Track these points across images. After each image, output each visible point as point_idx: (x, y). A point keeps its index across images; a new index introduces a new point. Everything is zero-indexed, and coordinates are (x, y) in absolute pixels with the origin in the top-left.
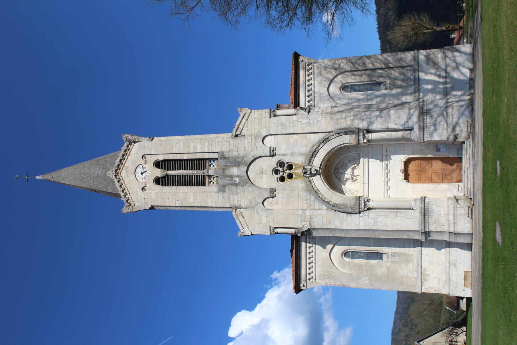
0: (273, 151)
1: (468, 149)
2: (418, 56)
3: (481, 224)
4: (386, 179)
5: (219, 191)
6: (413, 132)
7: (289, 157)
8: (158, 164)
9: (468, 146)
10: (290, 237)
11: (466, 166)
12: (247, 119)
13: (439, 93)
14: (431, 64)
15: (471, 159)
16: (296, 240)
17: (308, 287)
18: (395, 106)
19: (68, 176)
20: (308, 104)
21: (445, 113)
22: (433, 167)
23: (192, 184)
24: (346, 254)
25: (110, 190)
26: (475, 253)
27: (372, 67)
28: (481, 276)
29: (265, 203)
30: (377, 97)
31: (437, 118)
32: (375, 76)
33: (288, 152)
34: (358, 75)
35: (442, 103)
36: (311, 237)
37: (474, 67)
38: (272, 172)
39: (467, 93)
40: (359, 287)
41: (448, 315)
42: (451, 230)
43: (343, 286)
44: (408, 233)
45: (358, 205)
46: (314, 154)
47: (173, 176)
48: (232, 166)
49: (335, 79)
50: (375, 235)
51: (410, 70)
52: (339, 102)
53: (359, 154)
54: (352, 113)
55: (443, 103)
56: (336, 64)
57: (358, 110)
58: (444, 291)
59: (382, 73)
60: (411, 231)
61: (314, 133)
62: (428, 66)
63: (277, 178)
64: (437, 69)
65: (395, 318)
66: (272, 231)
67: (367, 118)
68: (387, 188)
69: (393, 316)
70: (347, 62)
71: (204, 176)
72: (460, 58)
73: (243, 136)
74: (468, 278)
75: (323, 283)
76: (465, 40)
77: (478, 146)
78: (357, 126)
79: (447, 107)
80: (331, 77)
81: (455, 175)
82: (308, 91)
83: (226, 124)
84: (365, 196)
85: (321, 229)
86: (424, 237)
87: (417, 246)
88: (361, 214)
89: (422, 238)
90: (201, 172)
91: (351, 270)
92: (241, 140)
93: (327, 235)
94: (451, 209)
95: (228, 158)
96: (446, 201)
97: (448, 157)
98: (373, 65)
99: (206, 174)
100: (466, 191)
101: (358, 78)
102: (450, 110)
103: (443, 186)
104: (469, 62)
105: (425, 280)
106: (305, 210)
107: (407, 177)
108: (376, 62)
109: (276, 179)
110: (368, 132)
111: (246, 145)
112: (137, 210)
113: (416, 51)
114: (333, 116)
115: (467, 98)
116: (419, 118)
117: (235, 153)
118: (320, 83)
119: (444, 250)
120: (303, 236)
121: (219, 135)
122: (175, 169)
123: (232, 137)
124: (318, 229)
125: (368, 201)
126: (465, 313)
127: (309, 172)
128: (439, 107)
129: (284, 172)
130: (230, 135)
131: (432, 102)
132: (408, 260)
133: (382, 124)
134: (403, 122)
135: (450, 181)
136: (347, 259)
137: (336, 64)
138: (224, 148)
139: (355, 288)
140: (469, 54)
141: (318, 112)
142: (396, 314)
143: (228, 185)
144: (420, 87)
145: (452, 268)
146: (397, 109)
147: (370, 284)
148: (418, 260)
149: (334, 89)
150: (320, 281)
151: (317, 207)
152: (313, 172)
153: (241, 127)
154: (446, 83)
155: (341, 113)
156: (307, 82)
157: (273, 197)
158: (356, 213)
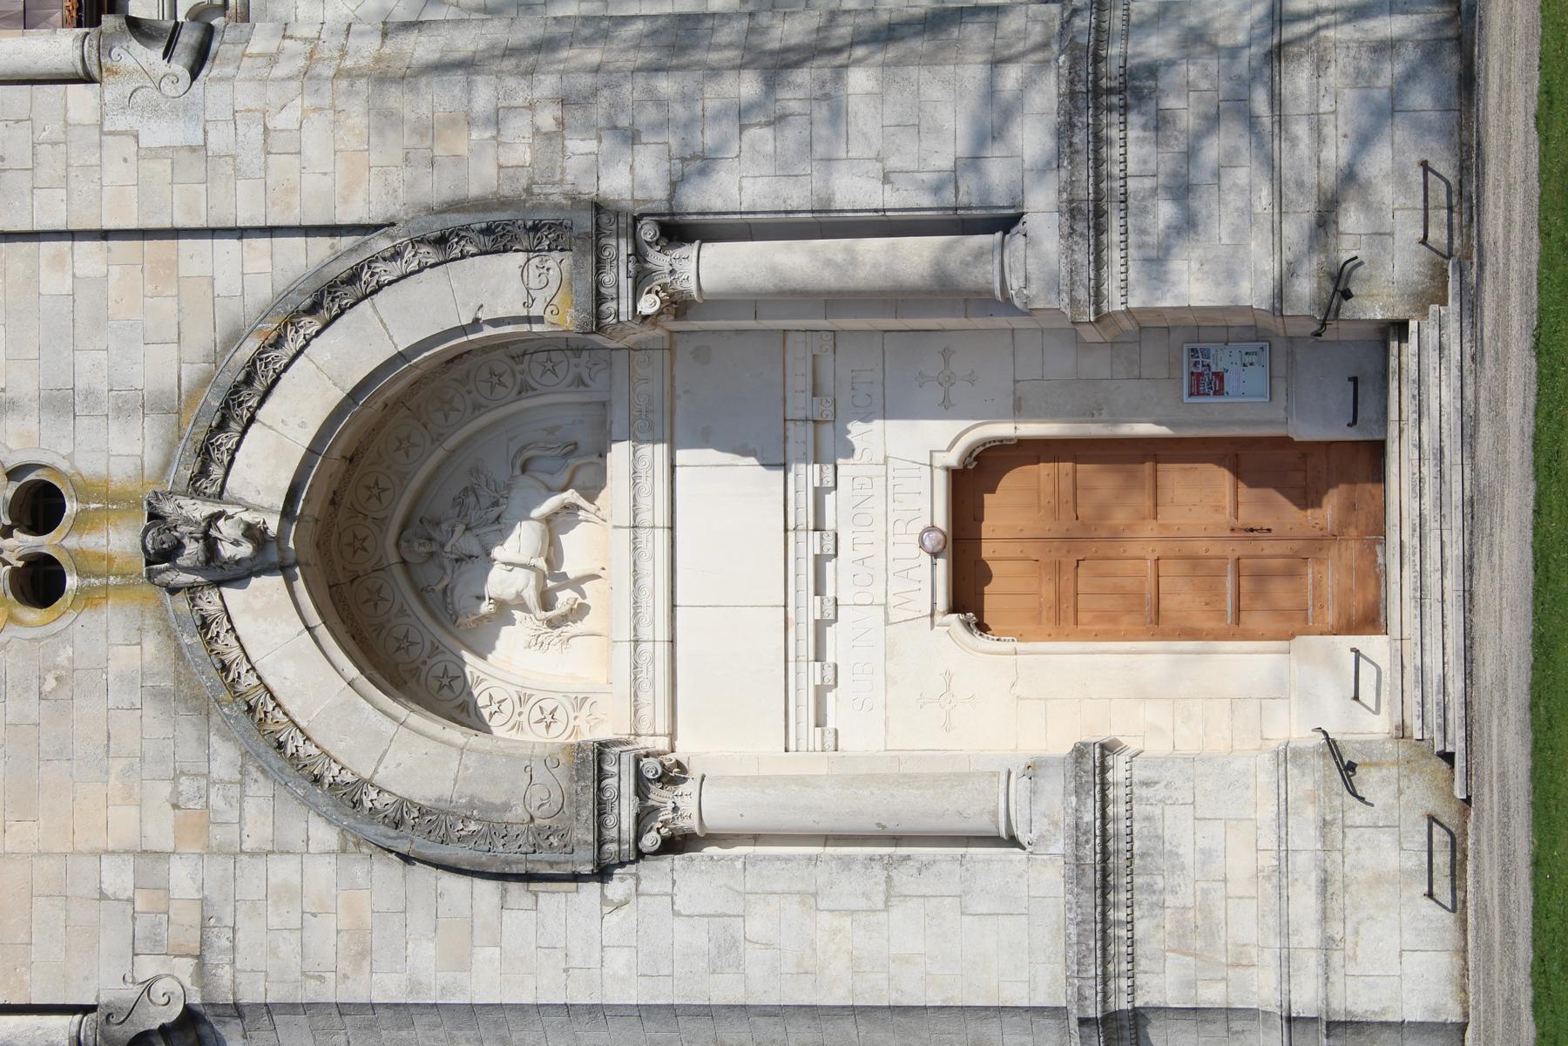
4: (812, 608)
6: (1016, 242)
9: (1432, 357)
22: (1168, 515)
45: (587, 812)
46: (237, 401)
53: (604, 404)
54: (547, 84)
57: (593, 56)
60: (1001, 1010)
61: (241, 232)
67: (657, 127)
68: (813, 674)
78: (587, 189)
81: (1330, 578)
85: (292, 1008)
88: (617, 887)
96: (1266, 779)
97: (1285, 442)
100: (1413, 696)
103: (1246, 663)
107: (967, 595)
110: (678, 231)
114: (395, 98)
124: (269, 1008)
125: (672, 776)
127: (193, 549)
133: (785, 170)
141: (272, 59)
151: (258, 831)
152: (227, 551)
155: (459, 76)
158: (576, 878)
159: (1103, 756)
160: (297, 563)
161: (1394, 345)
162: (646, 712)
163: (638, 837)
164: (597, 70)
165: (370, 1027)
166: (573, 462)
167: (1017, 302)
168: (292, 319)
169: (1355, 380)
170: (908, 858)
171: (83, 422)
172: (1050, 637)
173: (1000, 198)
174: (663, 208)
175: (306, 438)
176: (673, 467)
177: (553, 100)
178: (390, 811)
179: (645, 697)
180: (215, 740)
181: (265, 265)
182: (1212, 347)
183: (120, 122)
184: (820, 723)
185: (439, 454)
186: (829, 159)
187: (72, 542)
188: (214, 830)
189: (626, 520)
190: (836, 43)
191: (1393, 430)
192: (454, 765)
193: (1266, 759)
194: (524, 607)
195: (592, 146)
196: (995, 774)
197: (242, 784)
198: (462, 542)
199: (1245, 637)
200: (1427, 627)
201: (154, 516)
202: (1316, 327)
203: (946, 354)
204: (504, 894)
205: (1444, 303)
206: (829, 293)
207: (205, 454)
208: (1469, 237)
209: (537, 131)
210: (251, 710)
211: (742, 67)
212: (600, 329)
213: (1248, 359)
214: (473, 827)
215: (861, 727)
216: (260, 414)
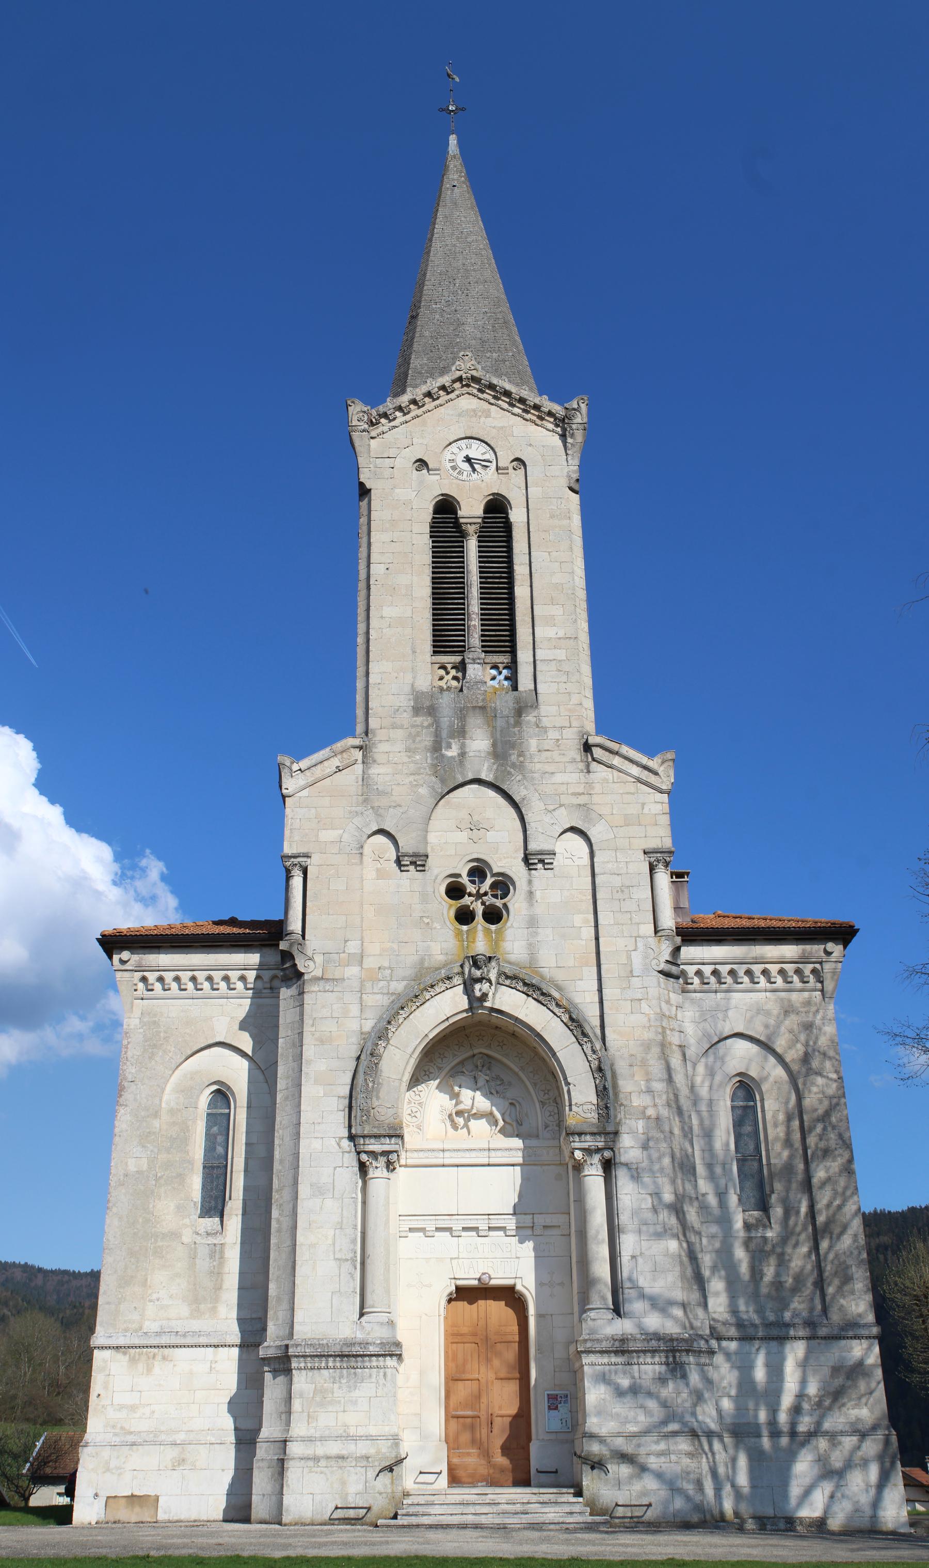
0: (541, 861)
1: (557, 1509)
2: (856, 1337)
3: (312, 1553)
4: (457, 1226)
5: (417, 696)
6: (610, 1315)
7: (524, 912)
8: (497, 507)
9: (567, 1509)
10: (277, 916)
11: (502, 1499)
12: (639, 780)
13: (740, 1409)
14: (839, 1381)
15: (526, 1519)
16: (268, 937)
17: (119, 974)
18: (692, 1256)
19: (459, 232)
20: (691, 970)
21: (673, 1427)
22: (498, 1384)
23: (438, 613)
24: (222, 1095)
25: (416, 362)
26: (212, 1534)
27: (815, 1181)
28: (141, 1553)
29: (380, 838)
30: (722, 1196)
31: (658, 1398)
32: (788, 1190)
33: (539, 910)
34: (788, 1133)
35: (707, 1416)
36: (276, 983)
37: (833, 1533)
38: (477, 860)
39: (744, 1509)
40: (117, 1139)
41: (14, 1445)
42: (294, 1449)
43: (121, 1090)
44: (286, 1298)
45: (376, 1131)
46: (536, 990)
47: (461, 554)
48: (493, 735)
49: (772, 1060)
50: (280, 1190)
51: (812, 1309)
52: (701, 1069)
53: (537, 1136)
54: (665, 1112)
55: (708, 1420)
56: (822, 1062)
57: (677, 1131)
58: (95, 1426)
59: (798, 1212)
60: (293, 1309)
61: (600, 990)
62: (826, 1371)
63: (459, 876)
64: (819, 1404)
65: (14, 1265)
66: (296, 861)
67: (650, 1157)
68: (431, 1227)
69: (20, 1258)
70: (831, 1098)
71: (461, 650)
72: (861, 1483)
73: (588, 766)
74: (137, 1509)
75: (132, 1022)
76: (919, 1507)
77: (567, 1542)
78: (623, 1129)
79: (694, 1434)
80: (780, 1045)
81: (472, 1460)
82: (732, 973)
83: (625, 714)
84: (403, 1155)
85: (302, 1014)
86: (271, 1353)
87: (242, 1331)
88: (346, 1144)
89: (269, 1347)
90: (475, 639)
91: (172, 1112)
92: (573, 761)
93: (282, 1032)
94: (363, 1448)
95: (518, 723)
96: (386, 1430)
97: (529, 1439)
98: (823, 1184)
99: (469, 656)
100: (421, 1500)
101: (781, 1131)
102: (683, 1445)
103: (435, 1421)
104: (850, 1518)
105: (133, 1361)
106: (361, 963)
108: (835, 1193)
110: (608, 1166)
111: (559, 778)
112: (358, 449)
113: (875, 1330)
114: (656, 1050)
115: (728, 1506)
116: (657, 1336)
117: (533, 744)
118: (759, 1010)
119: (228, 1423)
120: (279, 958)
121: (589, 693)
122: (483, 558)
123: (584, 734)
124: (302, 1005)
125: (390, 1166)
126: (23, 1504)
127: (478, 973)
128: (695, 1405)
129: (479, 896)
130: (591, 727)
131: (709, 1382)
132: (201, 1299)
133: (635, 1213)
135: (452, 1442)
136: (204, 1098)
137: (822, 1062)
138: (550, 710)
139: (114, 1127)
140: (874, 1517)
141: (668, 1002)
142: (26, 1268)
143: (437, 723)
144: (757, 1343)
145: (171, 1453)
146: (681, 1263)
147: (126, 1175)
148: (199, 1334)
149: (741, 1055)
150: (137, 1013)
151: (370, 1000)
152: (477, 986)
153: (616, 761)
154: (775, 1434)
155: (666, 1076)
156: (762, 967)
157: (398, 862)
158: (350, 1127)
159: (396, 1355)
160: (473, 1014)
161: (572, 1491)
162: (415, 1155)
163: (365, 1152)
164: (671, 1132)
165: (294, 1045)
166: (514, 1124)
167: (584, 1315)
168: (567, 1011)
169: (556, 1472)
171: (526, 931)
172: (446, 1331)
174: (617, 1161)
176: (513, 1165)
177: (658, 1114)
178: (377, 1051)
179: (421, 1154)
180: (405, 983)
181: (588, 1000)
182: (568, 1405)
183: (640, 944)
184: (411, 1230)
185: (516, 1070)
186: (640, 1232)
189: (492, 1146)
190: (688, 1234)
191: (535, 1490)
192: (394, 1077)
193: (395, 1430)
194: (457, 1104)
195: (641, 1130)
197: (388, 993)
199: (447, 1421)
200: (451, 1506)
201: (490, 959)
202: (578, 1453)
203: (562, 1284)
204: (344, 1097)
205: (591, 1515)
207: (514, 978)
208: (619, 1527)
209: (645, 1108)
210: (416, 997)
211: (676, 1194)
212: (568, 1134)
213: (564, 1421)
214: (371, 1085)
216: (530, 999)
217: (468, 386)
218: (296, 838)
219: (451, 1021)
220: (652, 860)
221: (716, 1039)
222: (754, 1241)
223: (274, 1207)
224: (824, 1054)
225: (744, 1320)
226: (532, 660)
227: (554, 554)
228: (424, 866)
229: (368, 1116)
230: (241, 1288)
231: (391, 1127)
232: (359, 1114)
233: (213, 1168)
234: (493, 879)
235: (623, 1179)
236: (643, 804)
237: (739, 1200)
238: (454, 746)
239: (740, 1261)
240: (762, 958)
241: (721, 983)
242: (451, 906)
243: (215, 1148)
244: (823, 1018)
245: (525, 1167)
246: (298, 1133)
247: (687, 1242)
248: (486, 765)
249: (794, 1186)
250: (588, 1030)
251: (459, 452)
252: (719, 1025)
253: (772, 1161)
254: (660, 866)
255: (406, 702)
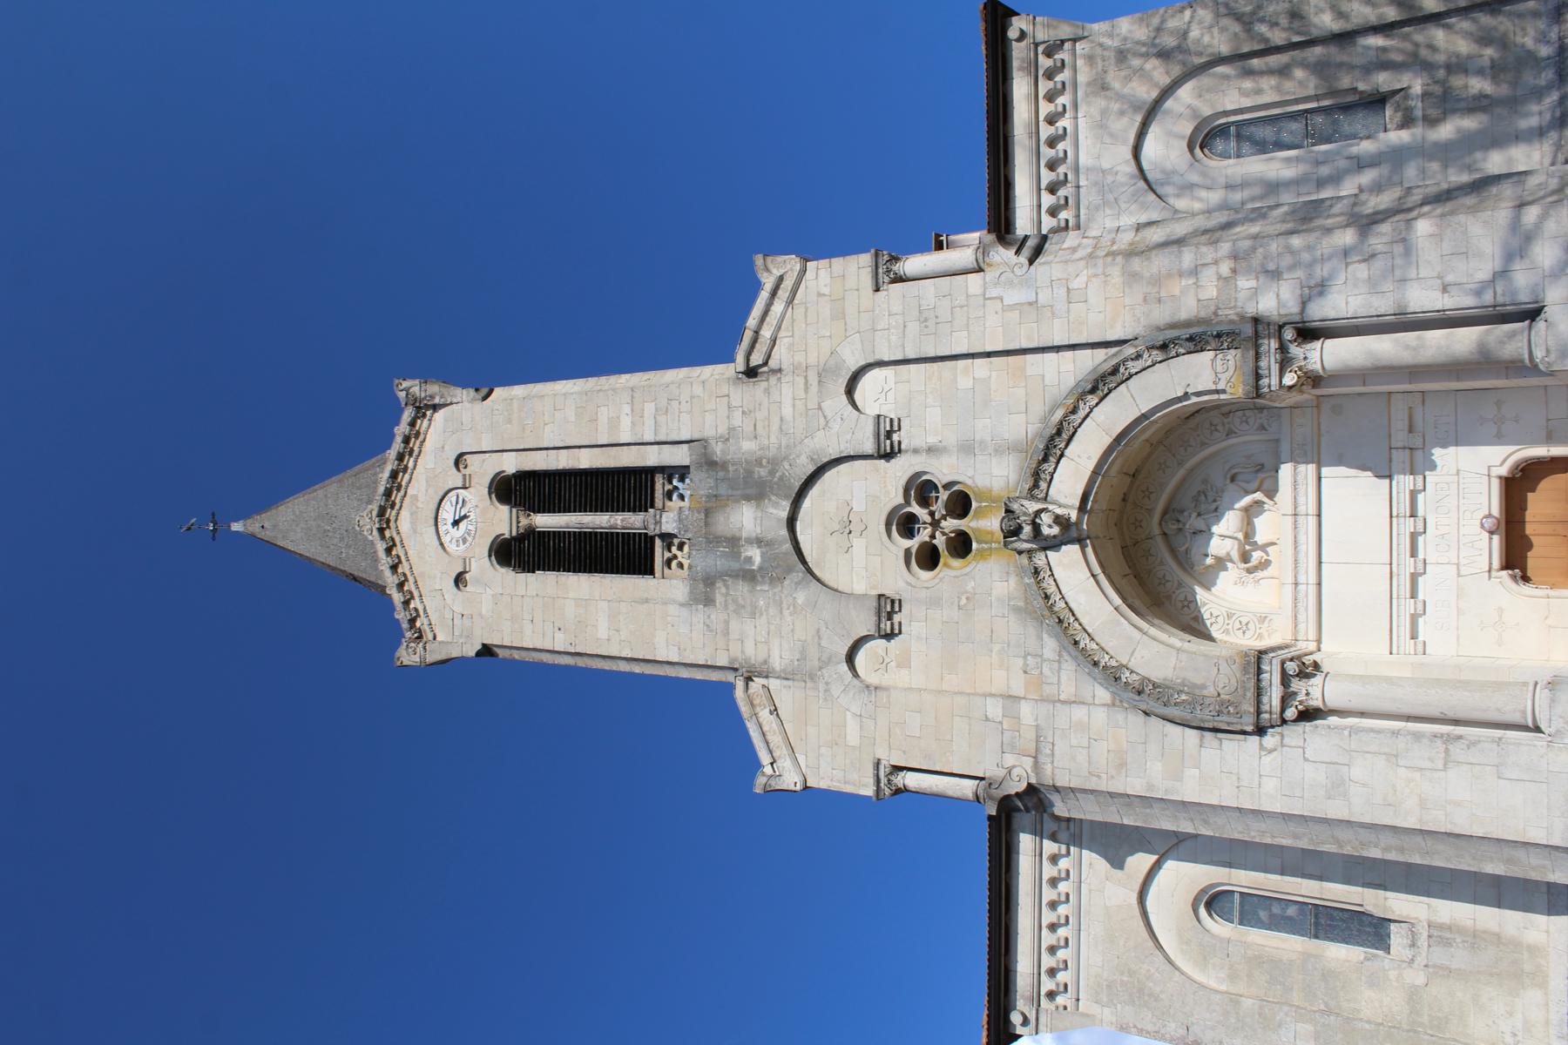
0: (889, 435)
4: (1409, 566)
6: (1540, 325)
8: (510, 489)
12: (790, 302)
18: (1445, 196)
24: (1214, 901)
29: (861, 659)
30: (1360, 164)
34: (1270, 72)
38: (888, 525)
45: (1250, 694)
46: (1053, 444)
48: (737, 501)
49: (1169, 104)
50: (1338, 842)
52: (1181, 204)
53: (1277, 441)
54: (1225, 248)
57: (1255, 229)
59: (1384, 50)
60: (1526, 844)
61: (1057, 349)
63: (908, 552)
66: (884, 780)
67: (1292, 268)
70: (1218, 15)
71: (649, 541)
78: (1251, 310)
80: (1148, 94)
82: (1052, 166)
83: (704, 322)
85: (1084, 791)
88: (1270, 740)
91: (1233, 977)
92: (767, 391)
93: (1115, 819)
95: (723, 466)
98: (1341, 15)
101: (1267, 83)
109: (902, 554)
110: (1308, 334)
111: (787, 411)
112: (443, 657)
114: (1136, 264)
117: (748, 446)
118: (1101, 126)
127: (1027, 529)
132: (1517, 970)
133: (1373, 285)
134: (1483, 272)
136: (1218, 927)
138: (710, 425)
141: (1074, 250)
149: (1164, 148)
151: (1067, 691)
152: (1046, 531)
153: (766, 333)
155: (1175, 248)
157: (889, 636)
158: (1244, 733)
162: (1302, 627)
163: (1283, 710)
164: (1255, 237)
165: (1129, 805)
166: (1261, 475)
167: (1541, 367)
168: (1081, 397)
170: (1460, 737)
173: (1524, 297)
174: (1297, 319)
175: (1091, 466)
176: (1319, 479)
179: (1301, 618)
180: (1045, 636)
181: (1070, 367)
184: (1414, 636)
185: (1182, 472)
186: (1404, 280)
187: (973, 524)
188: (1045, 687)
189: (1290, 511)
190: (1410, 205)
192: (1174, 660)
194: (1231, 561)
195: (1253, 283)
196: (1525, 684)
198: (1194, 522)
201: (1008, 511)
203: (1499, 404)
206: (1408, 367)
207: (1036, 475)
210: (1060, 621)
211: (1347, 226)
212: (1259, 396)
214: (1184, 697)
215: (1445, 641)
216: (1067, 452)
217: (388, 521)
218: (856, 776)
219: (1097, 570)
220: (887, 279)
221: (1142, 184)
222: (1429, 112)
223: (1365, 854)
224: (1159, 30)
225: (1553, 117)
226: (656, 447)
227: (546, 418)
228: (893, 602)
229: (1230, 703)
230: (1499, 904)
231: (1245, 670)
232: (1224, 718)
233: (1317, 924)
234: (914, 503)
235: (1326, 309)
236: (820, 295)
237: (1368, 137)
238: (749, 554)
239: (1459, 131)
240: (1029, 125)
241: (1066, 180)
242: (946, 565)
243: (1290, 918)
244: (1111, 36)
245: (1323, 457)
246: (1253, 811)
247: (1422, 205)
248: (771, 510)
249: (1345, 58)
250: (1108, 366)
251: (451, 535)
252: (1123, 180)
253: (1311, 92)
254: (895, 268)
255: (700, 614)
